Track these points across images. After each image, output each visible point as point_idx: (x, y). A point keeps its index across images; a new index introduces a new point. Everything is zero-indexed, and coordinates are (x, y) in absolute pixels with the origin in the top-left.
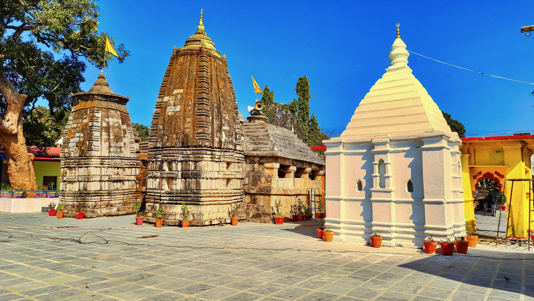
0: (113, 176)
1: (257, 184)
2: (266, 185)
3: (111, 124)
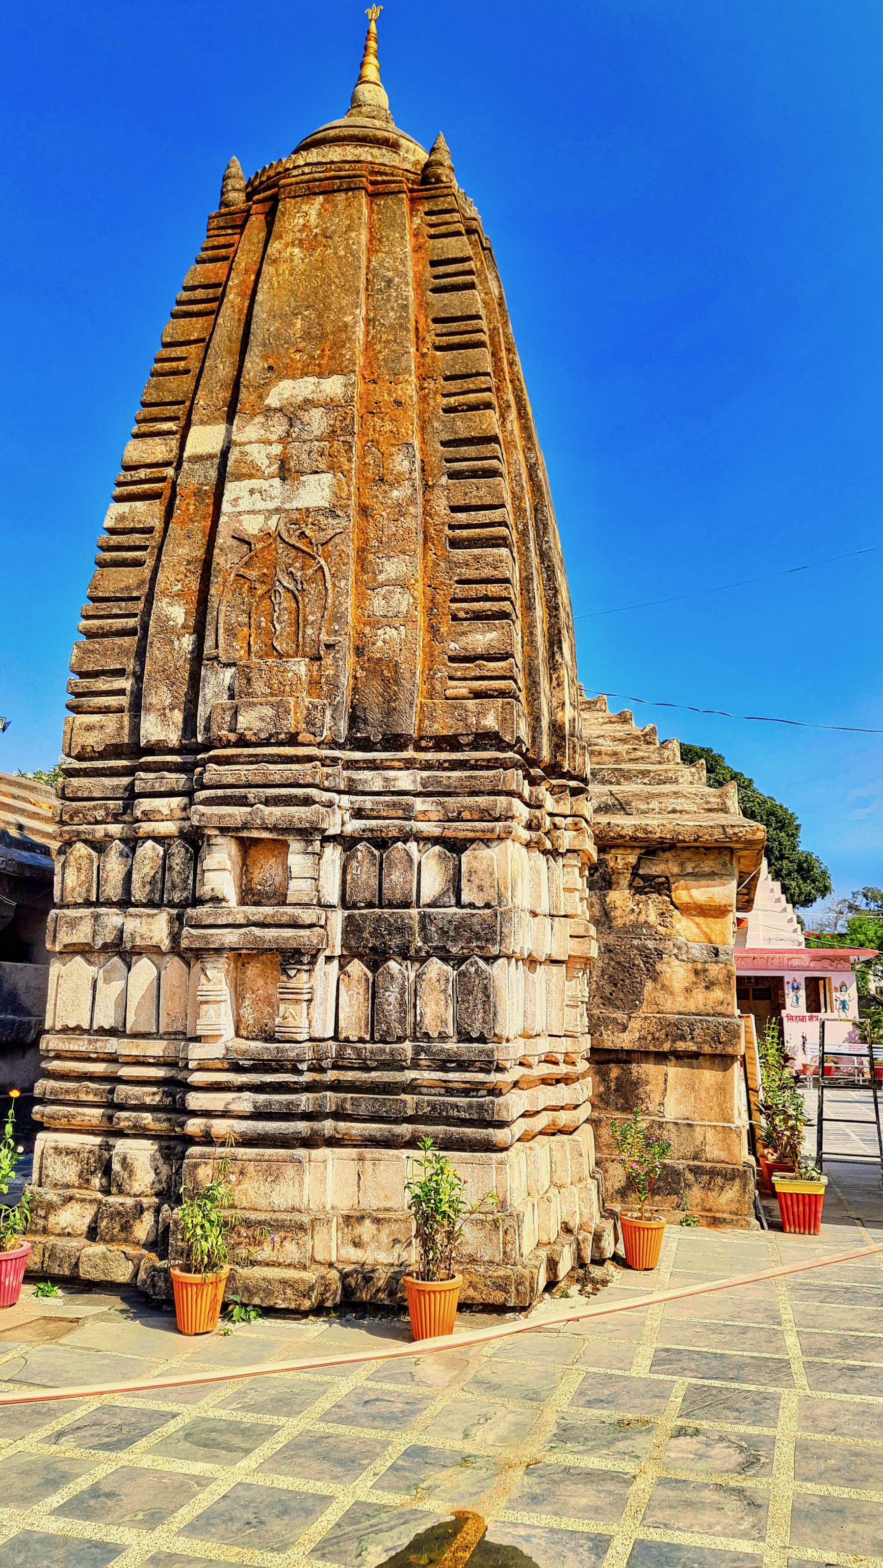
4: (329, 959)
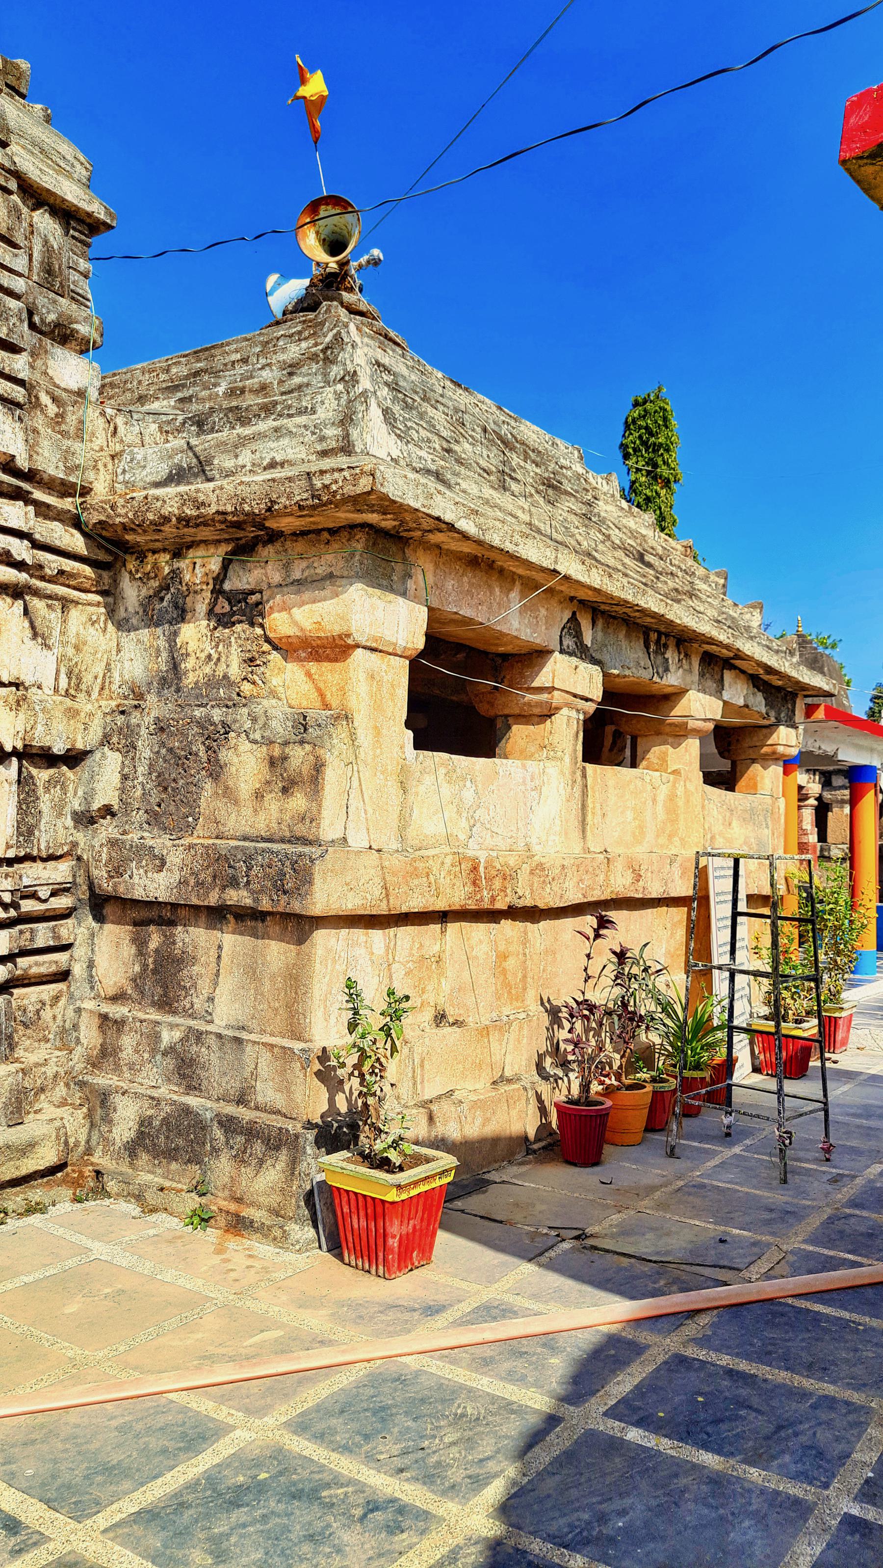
1: (192, 805)
2: (274, 814)
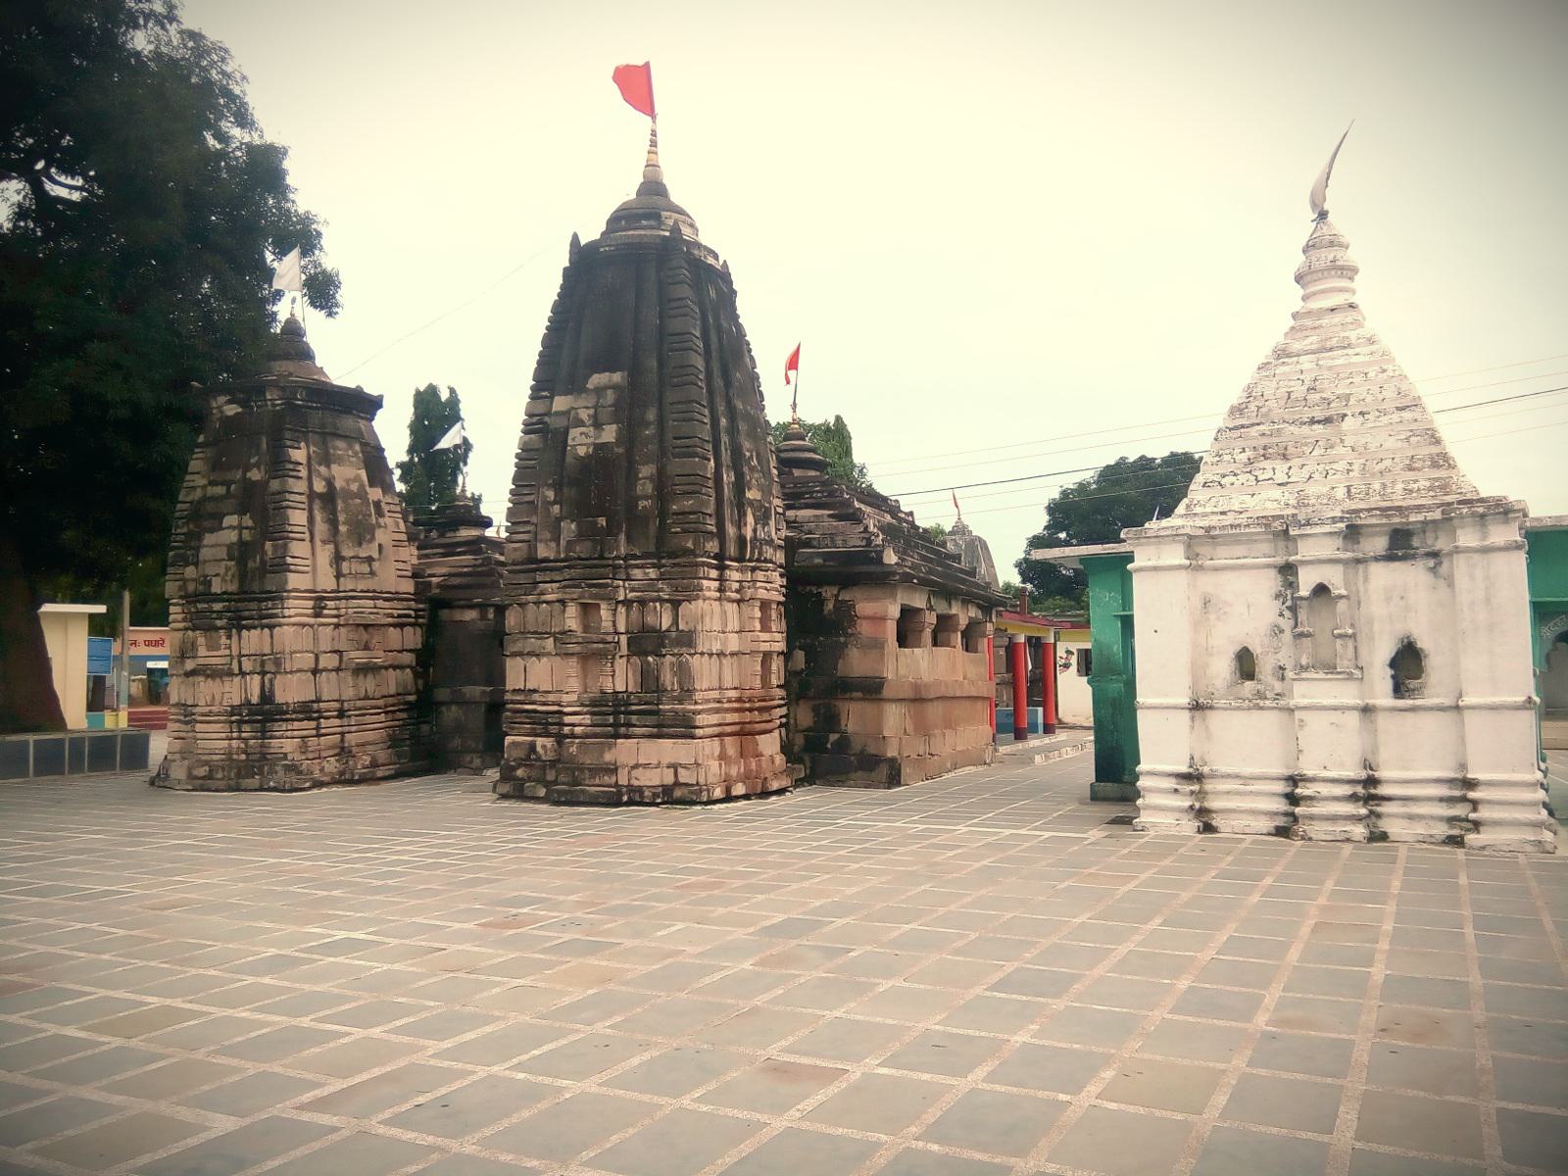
0: (353, 654)
3: (339, 484)
4: (621, 657)
